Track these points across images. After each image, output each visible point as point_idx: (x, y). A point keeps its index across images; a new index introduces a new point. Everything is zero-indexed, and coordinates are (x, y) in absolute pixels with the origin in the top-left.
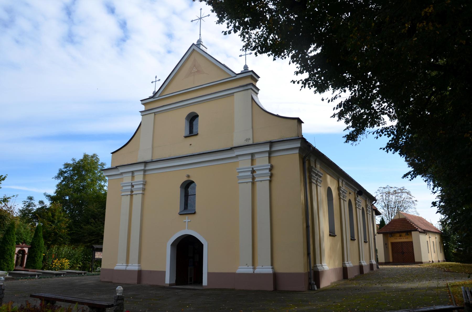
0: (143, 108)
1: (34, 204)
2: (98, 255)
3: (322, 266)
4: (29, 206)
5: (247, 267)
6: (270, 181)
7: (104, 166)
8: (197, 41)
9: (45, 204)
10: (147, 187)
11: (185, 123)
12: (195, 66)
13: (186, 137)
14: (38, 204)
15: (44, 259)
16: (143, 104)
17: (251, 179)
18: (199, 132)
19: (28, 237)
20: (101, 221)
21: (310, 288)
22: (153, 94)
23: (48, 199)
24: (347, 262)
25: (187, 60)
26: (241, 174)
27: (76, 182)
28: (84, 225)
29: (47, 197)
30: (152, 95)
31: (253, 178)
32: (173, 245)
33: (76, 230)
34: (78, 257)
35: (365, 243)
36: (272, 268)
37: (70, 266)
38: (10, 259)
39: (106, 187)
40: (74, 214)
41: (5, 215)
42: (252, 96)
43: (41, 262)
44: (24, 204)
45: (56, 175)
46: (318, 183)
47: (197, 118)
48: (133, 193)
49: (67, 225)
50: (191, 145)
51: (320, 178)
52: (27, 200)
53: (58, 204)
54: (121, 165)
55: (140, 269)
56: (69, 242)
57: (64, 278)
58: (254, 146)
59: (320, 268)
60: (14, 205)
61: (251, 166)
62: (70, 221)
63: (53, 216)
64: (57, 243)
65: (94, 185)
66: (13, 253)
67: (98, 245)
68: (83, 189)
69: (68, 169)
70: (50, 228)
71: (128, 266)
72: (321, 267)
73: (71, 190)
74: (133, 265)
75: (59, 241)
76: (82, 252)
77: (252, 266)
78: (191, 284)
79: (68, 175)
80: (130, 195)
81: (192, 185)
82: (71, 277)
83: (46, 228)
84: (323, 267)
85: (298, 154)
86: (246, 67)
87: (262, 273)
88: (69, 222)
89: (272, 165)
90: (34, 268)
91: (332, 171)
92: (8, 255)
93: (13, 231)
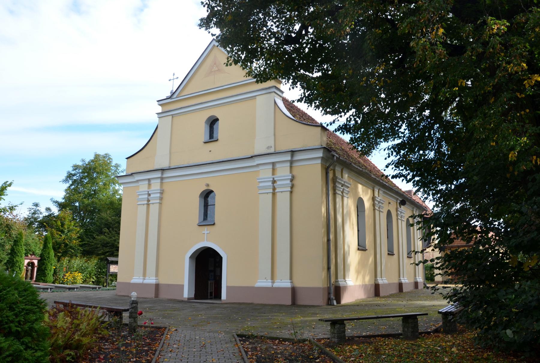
0: (160, 109)
1: (41, 211)
2: (113, 269)
3: (345, 281)
4: (34, 213)
5: (266, 281)
6: (291, 192)
7: (119, 168)
9: (53, 211)
10: (165, 196)
11: (205, 128)
12: (215, 64)
13: (205, 143)
14: (45, 211)
15: (55, 273)
16: (159, 105)
17: (272, 189)
18: (219, 138)
19: (37, 248)
20: (116, 231)
21: (329, 302)
22: (171, 93)
23: (56, 205)
24: (381, 279)
25: (207, 57)
26: (261, 185)
27: (87, 187)
28: (97, 235)
29: (54, 203)
30: (170, 95)
31: (274, 189)
32: (191, 257)
33: (88, 241)
34: (91, 271)
35: (408, 259)
36: (291, 282)
37: (83, 281)
38: (19, 272)
39: (121, 191)
40: (85, 222)
41: (12, 224)
42: (274, 100)
43: (52, 276)
44: (30, 211)
45: (64, 178)
46: (344, 194)
47: (217, 122)
48: (150, 203)
49: (78, 235)
50: (210, 151)
51: (347, 188)
52: (33, 207)
53: (67, 211)
54: (137, 172)
55: (158, 283)
56: (81, 254)
57: (78, 293)
59: (341, 283)
60: (20, 213)
61: (272, 175)
62: (82, 230)
63: (63, 225)
64: (68, 255)
65: (106, 189)
66: (22, 265)
67: (113, 257)
68: (95, 194)
69: (77, 171)
70: (60, 238)
71: (145, 279)
72: (344, 282)
73: (81, 195)
74: (150, 278)
75: (70, 253)
76: (95, 266)
77: (271, 280)
78: (211, 299)
79: (78, 178)
80: (147, 204)
81: (212, 195)
82: (85, 292)
83: (55, 239)
84: (346, 283)
87: (280, 287)
88: (80, 232)
89: (294, 175)
90: (45, 281)
91: (364, 179)
92: (17, 267)
93: (21, 242)
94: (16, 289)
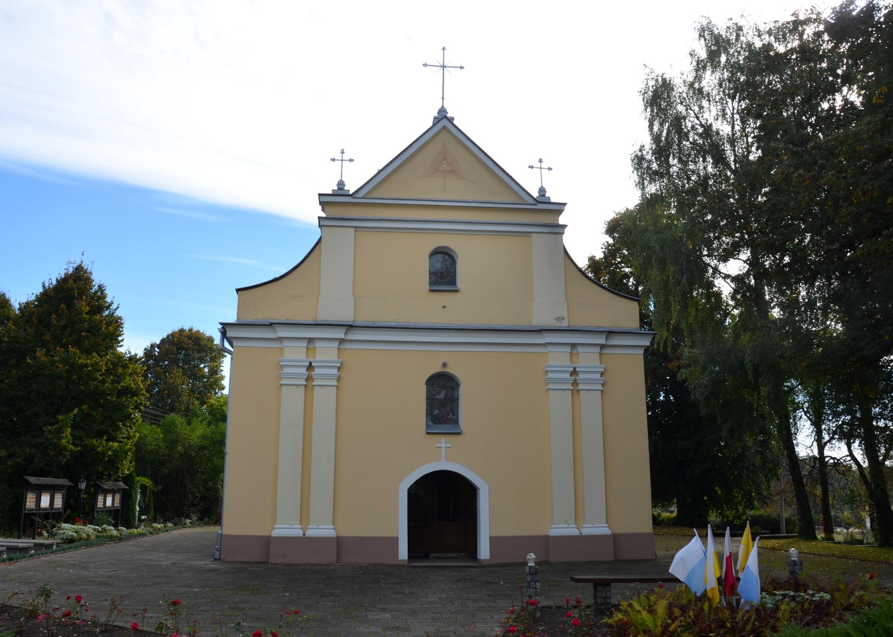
5: (567, 526)
8: (437, 111)
12: (445, 159)
50: (444, 307)
58: (582, 333)
85: (643, 356)
86: (341, 184)
87: (560, 535)
94: (882, 563)
